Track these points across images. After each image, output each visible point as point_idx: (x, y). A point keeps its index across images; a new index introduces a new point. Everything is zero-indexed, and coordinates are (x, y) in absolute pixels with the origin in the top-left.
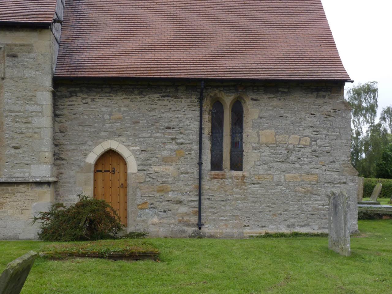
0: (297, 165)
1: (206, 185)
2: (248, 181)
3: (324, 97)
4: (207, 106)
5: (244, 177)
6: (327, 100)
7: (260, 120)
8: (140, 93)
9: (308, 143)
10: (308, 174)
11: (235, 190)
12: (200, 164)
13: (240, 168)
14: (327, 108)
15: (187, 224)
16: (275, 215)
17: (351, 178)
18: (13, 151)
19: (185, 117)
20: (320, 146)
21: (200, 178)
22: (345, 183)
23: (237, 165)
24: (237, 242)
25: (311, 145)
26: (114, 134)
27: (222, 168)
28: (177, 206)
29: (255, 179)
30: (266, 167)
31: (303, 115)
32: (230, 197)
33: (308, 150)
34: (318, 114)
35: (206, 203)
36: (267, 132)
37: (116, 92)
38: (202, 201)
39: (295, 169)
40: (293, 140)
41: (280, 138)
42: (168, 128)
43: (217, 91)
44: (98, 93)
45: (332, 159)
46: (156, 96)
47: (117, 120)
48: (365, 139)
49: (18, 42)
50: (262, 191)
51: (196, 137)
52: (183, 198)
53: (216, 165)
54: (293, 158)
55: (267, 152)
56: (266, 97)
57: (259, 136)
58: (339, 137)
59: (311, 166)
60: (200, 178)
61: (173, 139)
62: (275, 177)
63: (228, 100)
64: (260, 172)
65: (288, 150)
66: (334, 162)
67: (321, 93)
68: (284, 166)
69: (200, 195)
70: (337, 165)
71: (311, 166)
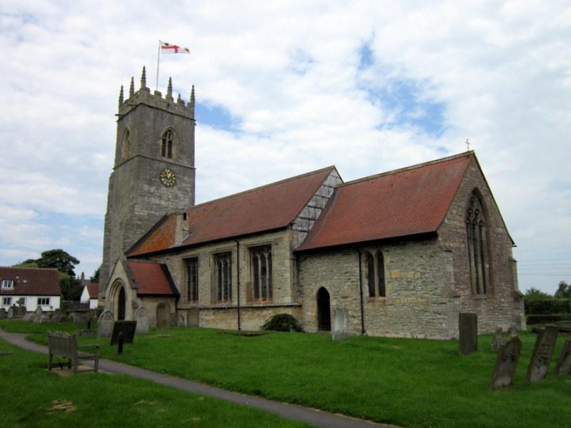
0: (414, 292)
1: (367, 306)
2: (387, 303)
3: (426, 244)
4: (364, 258)
5: (384, 301)
6: (428, 246)
7: (391, 264)
8: (333, 255)
9: (419, 277)
10: (422, 297)
11: (381, 309)
12: (362, 293)
13: (384, 296)
14: (429, 252)
15: (357, 330)
16: (404, 325)
17: (448, 299)
18: (278, 290)
19: (352, 266)
20: (427, 278)
21: (362, 302)
22: (445, 303)
23: (382, 293)
24: (450, 302)
25: (421, 278)
26: (323, 278)
27: (133, 322)
28: (353, 319)
29: (391, 302)
30: (396, 294)
31: (416, 258)
32: (378, 314)
33: (420, 281)
34: (424, 256)
35: (366, 318)
36: (396, 271)
37: (323, 255)
38: (364, 317)
39: (413, 294)
40: (410, 275)
41: (403, 274)
42: (346, 273)
43: (367, 249)
44: (315, 256)
45: (436, 287)
46: (340, 255)
47: (323, 271)
48: (127, 101)
49: (278, 237)
50: (395, 310)
51: (358, 277)
52: (355, 314)
53: (372, 294)
54: (411, 287)
55: (396, 284)
56: (393, 248)
57: (391, 274)
58: (438, 271)
59: (423, 292)
60: (362, 302)
61: (349, 279)
62: (402, 300)
63: (374, 253)
64: (394, 297)
65: (408, 282)
66: (436, 289)
67: (425, 242)
68: (407, 293)
69: (362, 312)
70: (439, 291)
71: (423, 292)
